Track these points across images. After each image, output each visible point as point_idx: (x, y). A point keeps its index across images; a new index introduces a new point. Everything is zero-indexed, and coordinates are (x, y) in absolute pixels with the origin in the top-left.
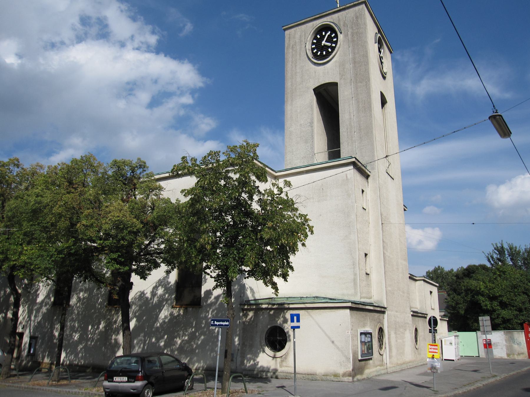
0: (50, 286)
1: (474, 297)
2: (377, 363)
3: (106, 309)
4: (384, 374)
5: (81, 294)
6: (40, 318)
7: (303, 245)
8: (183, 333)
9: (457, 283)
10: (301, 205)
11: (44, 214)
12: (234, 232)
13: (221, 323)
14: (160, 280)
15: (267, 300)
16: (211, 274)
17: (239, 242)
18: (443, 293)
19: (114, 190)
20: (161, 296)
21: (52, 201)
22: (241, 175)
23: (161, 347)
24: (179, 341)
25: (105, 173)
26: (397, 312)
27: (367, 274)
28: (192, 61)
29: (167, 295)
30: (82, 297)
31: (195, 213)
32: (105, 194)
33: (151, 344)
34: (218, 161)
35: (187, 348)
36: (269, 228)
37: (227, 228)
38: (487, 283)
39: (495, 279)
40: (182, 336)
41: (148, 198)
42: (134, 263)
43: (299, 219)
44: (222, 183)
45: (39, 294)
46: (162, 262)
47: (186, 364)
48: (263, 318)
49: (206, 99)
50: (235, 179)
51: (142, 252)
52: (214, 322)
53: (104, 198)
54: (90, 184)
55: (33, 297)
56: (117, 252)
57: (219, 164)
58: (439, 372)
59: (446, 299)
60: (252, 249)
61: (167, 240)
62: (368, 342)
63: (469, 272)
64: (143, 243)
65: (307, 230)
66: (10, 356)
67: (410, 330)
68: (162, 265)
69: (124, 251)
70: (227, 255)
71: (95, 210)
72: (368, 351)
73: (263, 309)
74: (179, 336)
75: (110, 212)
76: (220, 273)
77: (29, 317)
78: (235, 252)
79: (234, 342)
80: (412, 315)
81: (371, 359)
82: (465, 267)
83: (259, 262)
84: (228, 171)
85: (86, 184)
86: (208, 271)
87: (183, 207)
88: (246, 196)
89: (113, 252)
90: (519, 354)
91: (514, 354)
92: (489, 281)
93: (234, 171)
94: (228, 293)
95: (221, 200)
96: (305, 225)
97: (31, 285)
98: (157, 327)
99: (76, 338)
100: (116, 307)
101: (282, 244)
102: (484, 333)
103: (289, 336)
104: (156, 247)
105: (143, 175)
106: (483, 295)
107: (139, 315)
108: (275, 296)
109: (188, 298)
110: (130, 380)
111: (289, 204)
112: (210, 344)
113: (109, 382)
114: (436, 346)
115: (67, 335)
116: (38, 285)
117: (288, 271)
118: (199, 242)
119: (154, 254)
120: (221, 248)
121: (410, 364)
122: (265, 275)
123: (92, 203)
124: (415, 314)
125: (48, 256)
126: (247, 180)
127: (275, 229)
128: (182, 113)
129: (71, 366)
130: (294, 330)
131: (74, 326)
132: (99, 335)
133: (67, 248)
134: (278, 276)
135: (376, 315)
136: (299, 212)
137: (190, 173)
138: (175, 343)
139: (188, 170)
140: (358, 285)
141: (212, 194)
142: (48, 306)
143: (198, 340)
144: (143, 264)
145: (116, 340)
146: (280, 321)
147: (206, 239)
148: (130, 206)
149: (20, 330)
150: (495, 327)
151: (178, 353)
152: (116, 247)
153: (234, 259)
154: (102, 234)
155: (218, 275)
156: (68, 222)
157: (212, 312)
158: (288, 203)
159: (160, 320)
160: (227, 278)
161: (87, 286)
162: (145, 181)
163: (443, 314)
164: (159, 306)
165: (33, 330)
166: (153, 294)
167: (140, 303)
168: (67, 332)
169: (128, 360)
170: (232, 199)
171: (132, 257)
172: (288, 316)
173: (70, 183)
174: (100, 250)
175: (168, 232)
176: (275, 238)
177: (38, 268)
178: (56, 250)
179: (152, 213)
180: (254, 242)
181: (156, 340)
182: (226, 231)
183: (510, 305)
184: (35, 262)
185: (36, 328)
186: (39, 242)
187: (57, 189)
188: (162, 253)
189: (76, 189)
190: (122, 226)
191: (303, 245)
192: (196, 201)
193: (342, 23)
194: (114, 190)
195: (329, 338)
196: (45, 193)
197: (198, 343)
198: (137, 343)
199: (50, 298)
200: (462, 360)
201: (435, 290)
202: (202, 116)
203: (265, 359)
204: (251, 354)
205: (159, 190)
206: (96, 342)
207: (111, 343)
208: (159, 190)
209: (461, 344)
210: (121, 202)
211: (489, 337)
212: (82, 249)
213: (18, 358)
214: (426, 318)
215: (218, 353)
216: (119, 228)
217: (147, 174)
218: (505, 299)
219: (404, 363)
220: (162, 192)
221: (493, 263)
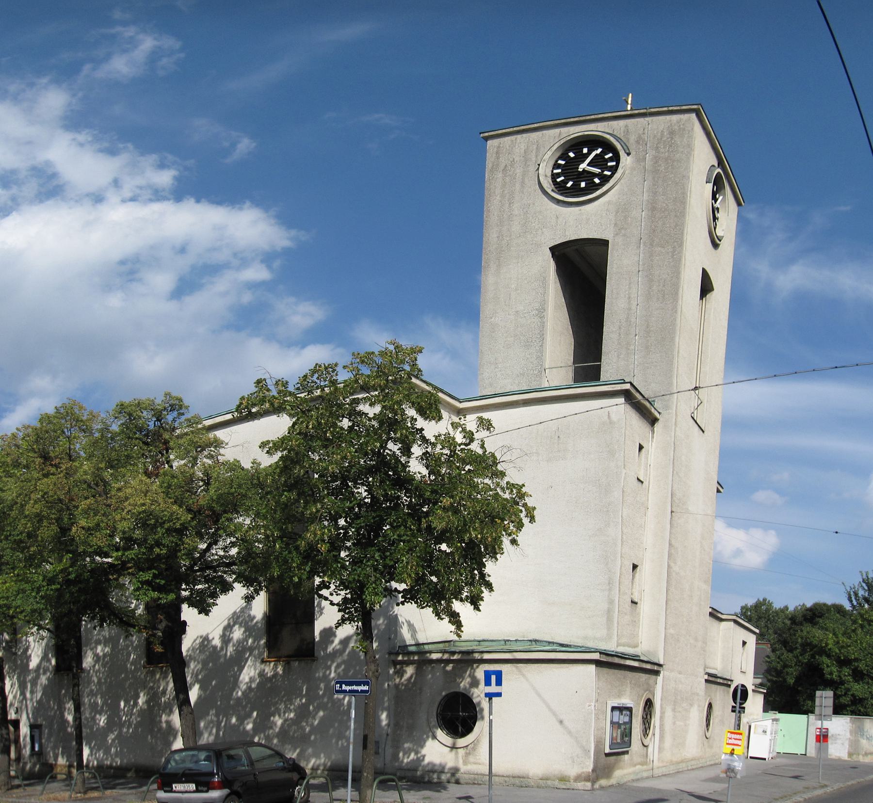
0: (45, 640)
1: (814, 658)
2: (637, 759)
3: (145, 671)
4: (647, 778)
5: (99, 649)
6: (39, 695)
7: (514, 542)
8: (286, 707)
9: (791, 631)
10: (512, 465)
11: (12, 520)
12: (374, 518)
13: (355, 688)
14: (235, 613)
15: (441, 646)
16: (330, 598)
17: (385, 536)
18: (764, 647)
19: (128, 457)
20: (239, 642)
21: (20, 495)
22: (383, 407)
23: (247, 732)
24: (279, 722)
25: (106, 429)
26: (680, 673)
27: (633, 602)
28: (259, 203)
29: (250, 641)
30: (101, 654)
31: (292, 485)
32: (112, 467)
33: (229, 727)
34: (334, 383)
35: (295, 732)
36: (444, 508)
37: (359, 509)
38: (840, 635)
39: (854, 631)
40: (285, 713)
41: (195, 464)
42: (184, 586)
43: (508, 492)
44: (346, 423)
45: (30, 656)
46: (235, 581)
47: (294, 760)
48: (433, 677)
49: (294, 271)
50: (371, 415)
51: (195, 564)
52: (341, 687)
53: (111, 475)
54: (82, 453)
55: (22, 661)
56: (149, 569)
57: (336, 389)
58: (739, 776)
59: (768, 657)
60: (411, 549)
61: (242, 540)
62: (625, 723)
63: (814, 614)
64: (195, 548)
65: (523, 515)
66: (7, 757)
67: (699, 706)
68: (236, 585)
69: (163, 566)
70: (361, 562)
71: (99, 499)
72: (622, 738)
73: (432, 661)
74: (278, 712)
75: (127, 499)
76: (349, 596)
77: (23, 694)
78: (377, 556)
79: (380, 721)
80: (706, 681)
81: (627, 752)
82: (809, 605)
83: (424, 575)
84: (357, 402)
85: (74, 455)
86: (325, 592)
87: (267, 475)
88: (397, 447)
89: (143, 570)
90: (866, 754)
91: (858, 754)
92: (844, 634)
93: (369, 399)
94: (366, 633)
95: (344, 458)
96: (518, 504)
97: (14, 642)
98: (238, 699)
99: (102, 723)
100: (162, 667)
101: (471, 540)
102: (821, 717)
103: (482, 710)
104: (221, 553)
105: (180, 423)
106: (829, 656)
107: (204, 677)
108: (455, 638)
109: (289, 644)
110: (200, 788)
111: (487, 464)
112: (336, 725)
113: (165, 791)
114: (741, 734)
115: (86, 719)
116: (26, 641)
117: (482, 592)
118: (303, 539)
119: (218, 566)
120: (348, 549)
121: (693, 762)
122: (438, 598)
123: (91, 488)
124: (711, 679)
125: (33, 590)
126: (398, 417)
127: (456, 511)
128: (247, 298)
129: (100, 768)
130: (490, 699)
131: (96, 704)
132: (139, 716)
133: (62, 571)
134: (462, 600)
135: (644, 677)
136: (506, 479)
137: (277, 410)
138: (272, 725)
139: (272, 404)
140: (615, 622)
141: (326, 447)
142: (48, 674)
143: (314, 718)
144: (200, 587)
145: (168, 723)
146: (464, 684)
147: (317, 533)
148: (163, 483)
149: (12, 716)
150: (838, 710)
151: (279, 741)
152: (148, 560)
153: (376, 570)
154: (118, 540)
155: (345, 600)
156: (55, 528)
157: (338, 667)
158: (484, 461)
159: (241, 685)
160: (363, 605)
161: (106, 633)
162: (186, 434)
163: (759, 681)
164: (238, 661)
165: (33, 714)
166: (226, 639)
167: (202, 657)
168: (86, 714)
169: (193, 755)
170: (366, 454)
171: (181, 577)
172: (480, 673)
173: (46, 457)
174: (120, 568)
175: (241, 525)
176: (456, 529)
177: (22, 612)
178: (45, 577)
179: (207, 490)
180: (414, 536)
181: (237, 720)
182: (357, 516)
183: (868, 675)
184: (14, 604)
185: (37, 711)
186: (13, 568)
187: (24, 473)
188: (234, 564)
189: (57, 466)
190: (152, 522)
191: (514, 542)
192: (292, 461)
194: (128, 457)
195: (554, 714)
196: (6, 483)
197: (313, 724)
198: (206, 727)
199: (49, 661)
200: (778, 760)
201: (752, 640)
202: (292, 300)
203: (436, 750)
204: (411, 742)
205: (215, 447)
206: (136, 727)
207: (160, 729)
208: (215, 447)
209: (780, 734)
210: (144, 478)
211: (826, 724)
212: (89, 571)
213: (18, 759)
214: (729, 686)
215: (352, 740)
216: (148, 525)
217: (188, 420)
218: (862, 666)
219: (682, 762)
220: (222, 451)
221: (855, 603)
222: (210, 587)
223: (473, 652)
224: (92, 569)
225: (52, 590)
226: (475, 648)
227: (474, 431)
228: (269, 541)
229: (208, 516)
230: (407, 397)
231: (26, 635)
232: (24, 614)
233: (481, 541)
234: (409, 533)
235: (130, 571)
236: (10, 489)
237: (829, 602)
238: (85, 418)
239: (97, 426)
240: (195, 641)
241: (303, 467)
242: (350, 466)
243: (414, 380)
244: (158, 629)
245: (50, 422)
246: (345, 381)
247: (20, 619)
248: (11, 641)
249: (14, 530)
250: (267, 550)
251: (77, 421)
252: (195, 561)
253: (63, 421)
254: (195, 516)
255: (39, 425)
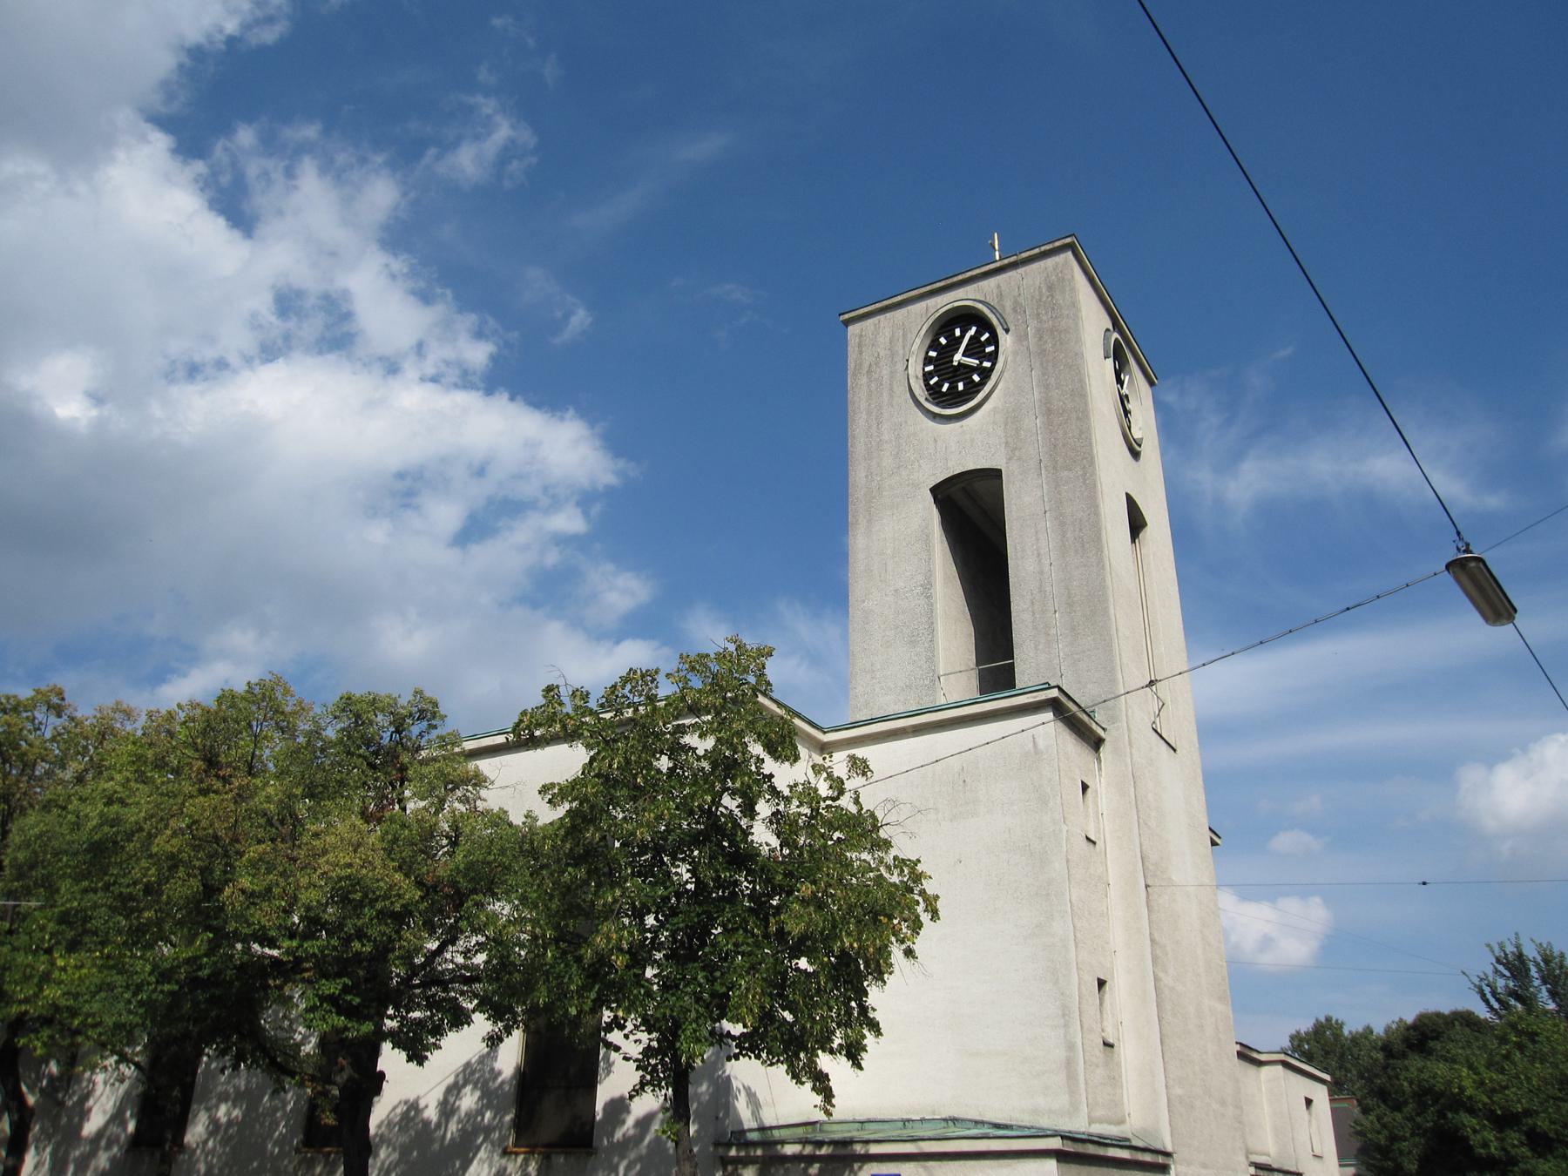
1: (1444, 1116)
3: (297, 1158)
5: (222, 1112)
7: (909, 953)
12: (698, 915)
14: (468, 1064)
15: (800, 1131)
17: (714, 945)
19: (341, 783)
22: (718, 740)
25: (316, 733)
26: (1204, 1166)
27: (1106, 1044)
28: (588, 414)
30: (224, 1120)
32: (312, 796)
34: (652, 699)
36: (803, 900)
37: (678, 900)
38: (1482, 1069)
39: (1507, 1057)
42: (390, 1012)
43: (896, 872)
44: (664, 763)
45: (90, 1110)
49: (620, 523)
50: (700, 752)
54: (271, 765)
55: (70, 1119)
56: (339, 975)
57: (655, 709)
64: (418, 950)
65: (920, 909)
70: (677, 987)
71: (280, 846)
73: (785, 1159)
75: (325, 852)
76: (655, 1044)
82: (1410, 1018)
84: (681, 730)
86: (615, 1037)
87: (544, 838)
88: (735, 803)
89: (326, 976)
92: (1490, 1065)
94: (679, 1108)
95: (660, 818)
100: (329, 1154)
101: (843, 951)
104: (460, 960)
105: (429, 741)
108: (821, 1116)
109: (552, 1124)
111: (863, 828)
116: (90, 1080)
117: (864, 1037)
118: (590, 945)
119: (452, 981)
122: (793, 1048)
123: (272, 825)
125: (127, 987)
127: (821, 906)
128: (552, 558)
133: (188, 961)
134: (832, 1052)
136: (893, 852)
137: (569, 736)
139: (564, 727)
141: (634, 799)
142: (115, 1149)
144: (416, 1014)
147: (611, 936)
152: (338, 960)
153: (698, 999)
154: (296, 920)
155: (648, 1052)
156: (195, 884)
160: (676, 1059)
162: (435, 760)
166: (447, 1109)
167: (403, 1139)
170: (691, 813)
173: (211, 762)
174: (287, 970)
176: (822, 933)
178: (155, 967)
179: (451, 854)
180: (758, 945)
182: (674, 912)
184: (86, 1008)
186: (103, 944)
187: (169, 781)
189: (225, 780)
190: (358, 896)
191: (909, 953)
192: (584, 819)
193: (1008, 304)
196: (133, 792)
199: (124, 1124)
201: (1321, 1095)
205: (475, 785)
208: (475, 785)
210: (359, 822)
212: (235, 967)
216: (350, 901)
217: (442, 738)
218: (1542, 1123)
220: (483, 793)
221: (1496, 1005)
222: (433, 1015)
223: (851, 1142)
224: (242, 964)
225: (162, 992)
226: (855, 1134)
227: (844, 777)
228: (537, 946)
229: (447, 896)
230: (751, 726)
231: (93, 1068)
232: (100, 1030)
233: (858, 953)
234: (750, 941)
235: (306, 975)
236: (138, 803)
237: (1446, 1009)
238: (288, 709)
239: (304, 726)
240: (394, 1108)
241: (598, 829)
242: (668, 831)
243: (761, 699)
244: (335, 1084)
245: (234, 705)
246: (668, 698)
247: (88, 1038)
248: (60, 1078)
249: (124, 875)
250: (533, 960)
251: (277, 711)
252: (414, 970)
253: (254, 708)
254: (427, 894)
255: (214, 706)
